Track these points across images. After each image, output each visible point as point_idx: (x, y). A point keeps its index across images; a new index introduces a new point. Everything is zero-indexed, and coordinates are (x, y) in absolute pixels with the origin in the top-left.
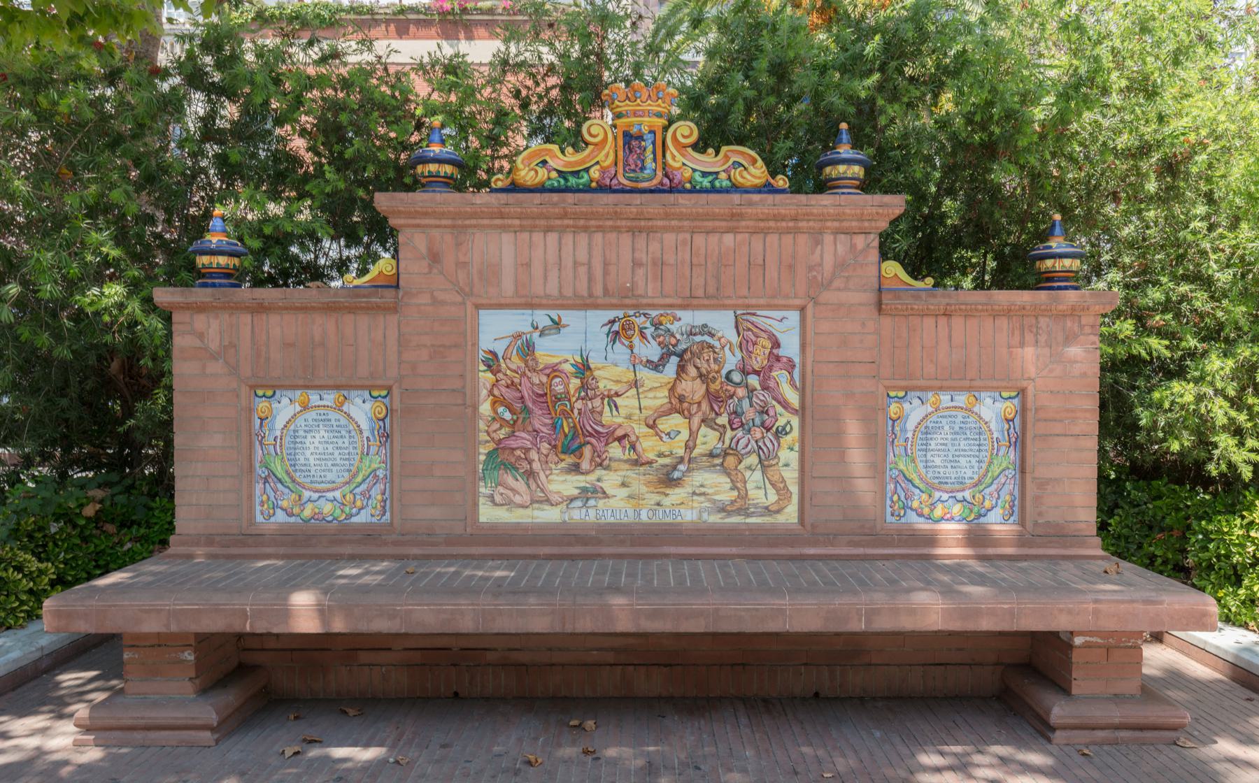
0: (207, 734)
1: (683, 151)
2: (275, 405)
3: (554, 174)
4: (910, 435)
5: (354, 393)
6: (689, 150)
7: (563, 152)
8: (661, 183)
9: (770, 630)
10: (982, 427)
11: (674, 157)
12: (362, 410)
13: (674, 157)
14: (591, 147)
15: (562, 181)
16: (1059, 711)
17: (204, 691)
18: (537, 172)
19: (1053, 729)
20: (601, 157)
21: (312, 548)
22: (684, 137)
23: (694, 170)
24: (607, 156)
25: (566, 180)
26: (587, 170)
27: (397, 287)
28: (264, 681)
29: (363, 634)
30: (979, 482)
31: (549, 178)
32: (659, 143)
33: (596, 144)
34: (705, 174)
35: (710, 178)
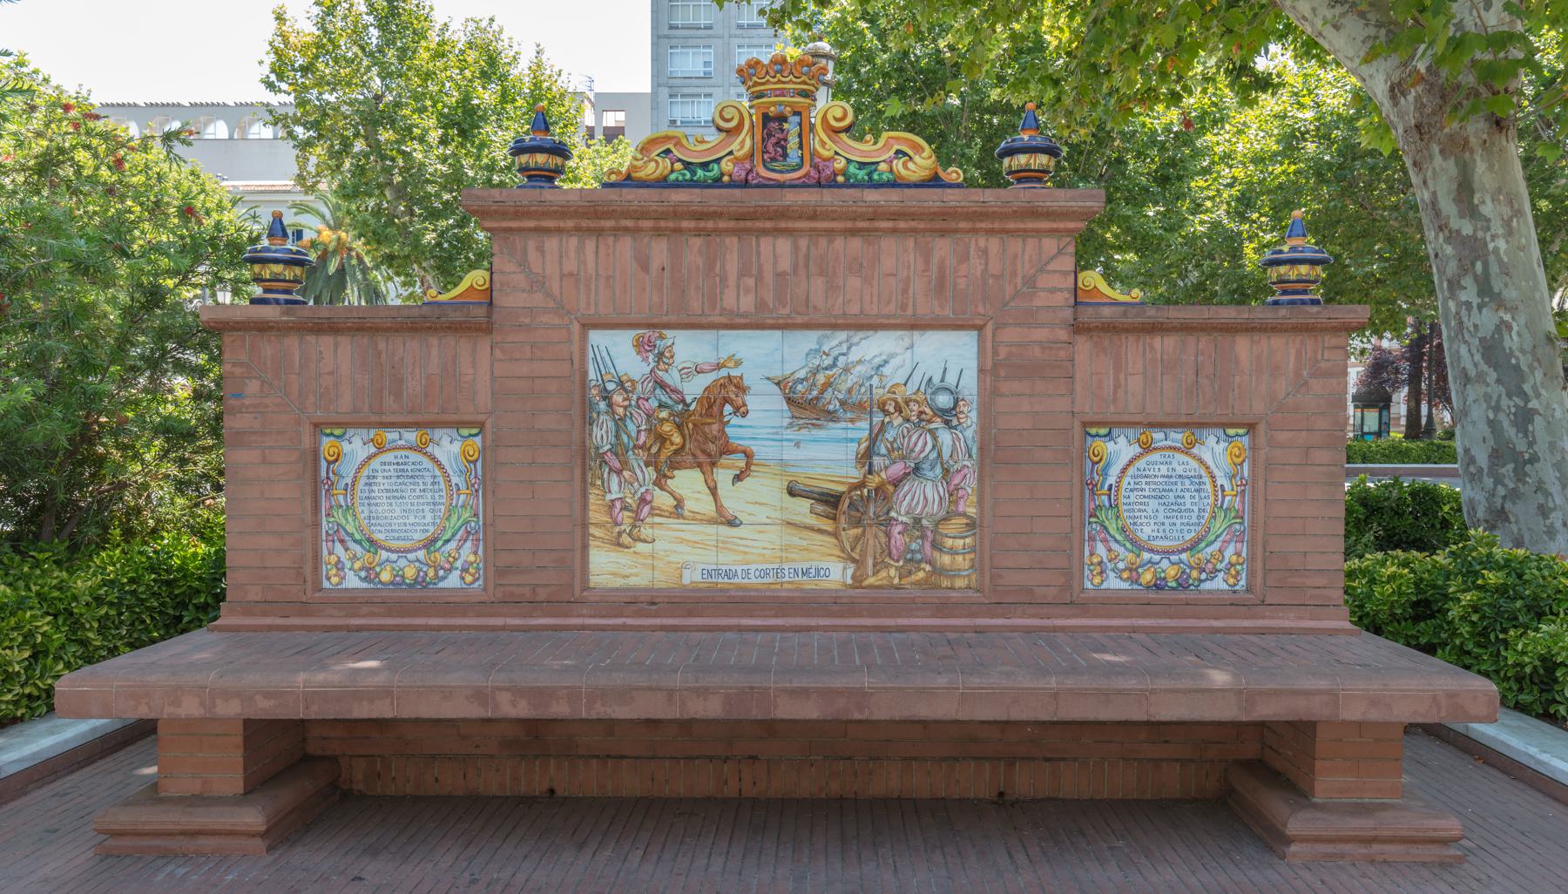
0: (258, 842)
3: (678, 166)
8: (807, 175)
11: (823, 144)
13: (823, 144)
15: (688, 176)
16: (1297, 823)
17: (256, 785)
19: (1289, 841)
20: (735, 146)
21: (402, 613)
22: (837, 120)
23: (849, 161)
25: (694, 173)
28: (320, 774)
31: (672, 171)
33: (728, 131)
34: (862, 165)
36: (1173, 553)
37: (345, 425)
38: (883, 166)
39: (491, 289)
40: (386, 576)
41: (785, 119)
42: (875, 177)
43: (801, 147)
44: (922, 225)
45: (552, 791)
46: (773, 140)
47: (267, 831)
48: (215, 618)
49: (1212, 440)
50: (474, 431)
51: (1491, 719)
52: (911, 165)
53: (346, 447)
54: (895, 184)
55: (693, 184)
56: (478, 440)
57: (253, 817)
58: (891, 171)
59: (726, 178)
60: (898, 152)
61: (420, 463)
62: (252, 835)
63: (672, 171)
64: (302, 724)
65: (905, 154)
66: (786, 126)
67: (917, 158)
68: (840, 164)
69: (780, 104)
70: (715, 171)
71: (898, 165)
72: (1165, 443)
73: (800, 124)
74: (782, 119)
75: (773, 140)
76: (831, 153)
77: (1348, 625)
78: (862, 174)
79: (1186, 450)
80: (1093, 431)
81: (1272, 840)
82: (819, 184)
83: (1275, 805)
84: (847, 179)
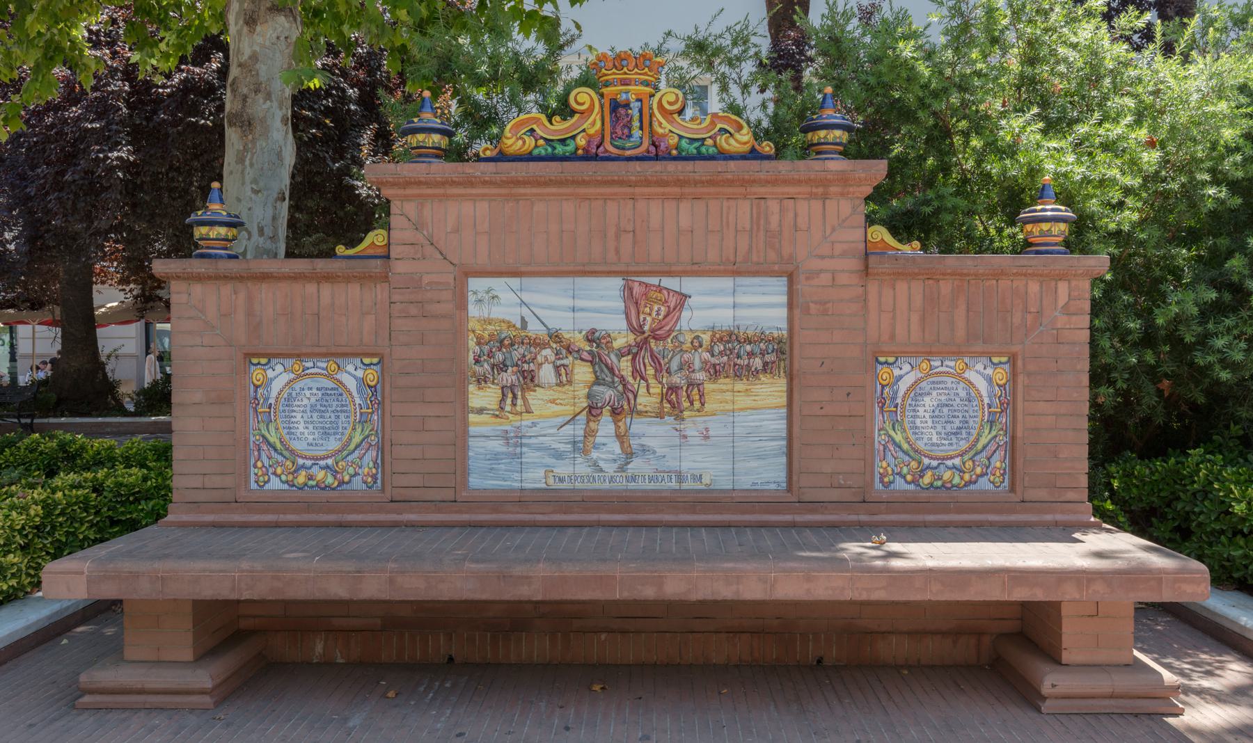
2: (270, 374)
3: (541, 142)
6: (676, 116)
12: (352, 375)
14: (577, 116)
15: (550, 150)
16: (1052, 682)
17: (204, 655)
18: (524, 142)
19: (1044, 698)
21: (318, 514)
22: (670, 103)
23: (681, 137)
24: (593, 124)
26: (574, 137)
27: (388, 257)
28: (259, 645)
31: (536, 146)
33: (582, 113)
34: (692, 140)
35: (697, 144)
37: (270, 356)
38: (709, 142)
39: (389, 244)
45: (451, 659)
47: (214, 688)
49: (350, 368)
50: (1004, 359)
52: (732, 141)
55: (553, 158)
56: (1007, 367)
58: (715, 145)
59: (580, 152)
60: (721, 130)
62: (202, 692)
65: (727, 131)
67: (737, 136)
68: (673, 141)
70: (570, 148)
71: (722, 141)
72: (941, 369)
78: (692, 149)
80: (255, 361)
82: (657, 158)
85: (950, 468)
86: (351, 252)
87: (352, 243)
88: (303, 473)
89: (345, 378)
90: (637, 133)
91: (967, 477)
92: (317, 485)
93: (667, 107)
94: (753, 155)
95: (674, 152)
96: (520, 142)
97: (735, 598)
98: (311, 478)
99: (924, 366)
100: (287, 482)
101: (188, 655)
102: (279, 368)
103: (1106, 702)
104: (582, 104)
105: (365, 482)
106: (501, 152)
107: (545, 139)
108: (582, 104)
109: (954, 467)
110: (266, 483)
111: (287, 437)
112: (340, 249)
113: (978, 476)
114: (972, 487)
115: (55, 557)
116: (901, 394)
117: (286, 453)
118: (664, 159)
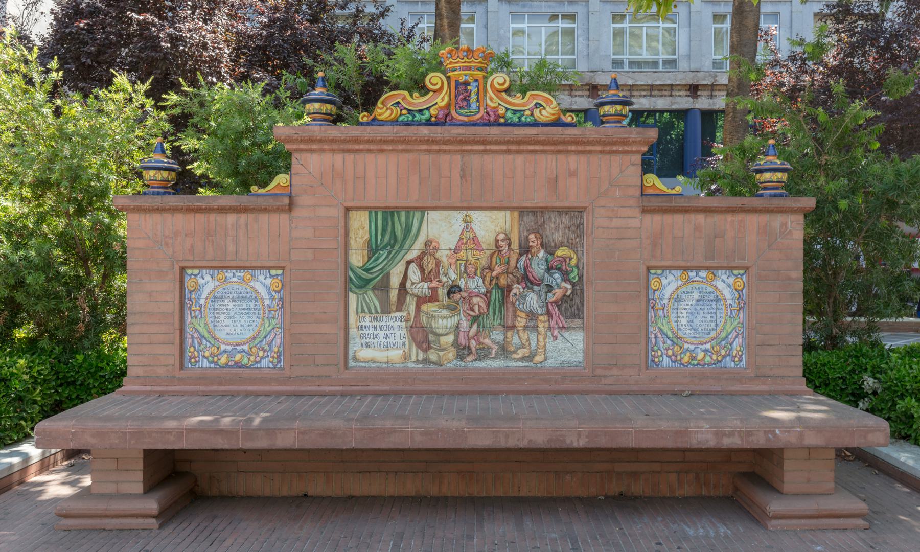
0: (154, 520)
1: (499, 94)
4: (665, 301)
5: (720, 272)
6: (503, 94)
7: (411, 96)
8: (482, 118)
9: (624, 445)
10: (255, 296)
11: (491, 99)
12: (263, 283)
13: (491, 99)
14: (431, 93)
15: (410, 118)
17: (150, 488)
18: (392, 110)
20: (438, 100)
21: (232, 383)
23: (507, 109)
24: (443, 100)
25: (414, 116)
28: (183, 480)
29: (463, 450)
30: (254, 338)
31: (401, 115)
32: (481, 87)
33: (435, 91)
34: (515, 112)
35: (518, 115)
36: (238, 345)
40: (223, 360)
41: (469, 84)
42: (523, 119)
43: (478, 101)
44: (326, 147)
46: (461, 96)
48: (120, 386)
49: (261, 278)
51: (885, 445)
53: (201, 281)
54: (536, 124)
56: (281, 278)
57: (152, 505)
58: (532, 115)
59: (433, 119)
61: (706, 288)
63: (401, 115)
64: (173, 451)
65: (541, 105)
66: (469, 88)
67: (548, 108)
69: (466, 75)
70: (426, 115)
73: (478, 87)
74: (467, 84)
75: (461, 96)
76: (496, 105)
77: (805, 388)
79: (708, 281)
81: (757, 517)
83: (761, 497)
84: (506, 120)
85: (239, 352)
86: (262, 191)
87: (263, 185)
88: (688, 354)
89: (258, 286)
90: (474, 106)
91: (714, 357)
92: (698, 364)
93: (498, 87)
94: (557, 123)
95: (502, 120)
96: (389, 112)
97: (718, 446)
98: (694, 358)
99: (220, 276)
100: (213, 362)
101: (139, 488)
102: (671, 277)
103: (140, 521)
104: (436, 85)
105: (272, 363)
106: (374, 119)
107: (408, 110)
108: (436, 85)
109: (706, 350)
110: (196, 362)
111: (675, 329)
112: (254, 188)
113: (724, 357)
114: (719, 365)
115: (46, 415)
116: (667, 297)
117: (212, 341)
118: (493, 125)
